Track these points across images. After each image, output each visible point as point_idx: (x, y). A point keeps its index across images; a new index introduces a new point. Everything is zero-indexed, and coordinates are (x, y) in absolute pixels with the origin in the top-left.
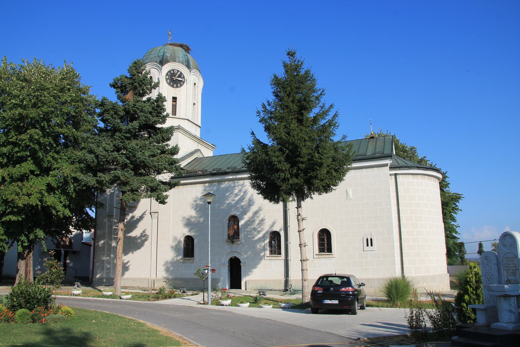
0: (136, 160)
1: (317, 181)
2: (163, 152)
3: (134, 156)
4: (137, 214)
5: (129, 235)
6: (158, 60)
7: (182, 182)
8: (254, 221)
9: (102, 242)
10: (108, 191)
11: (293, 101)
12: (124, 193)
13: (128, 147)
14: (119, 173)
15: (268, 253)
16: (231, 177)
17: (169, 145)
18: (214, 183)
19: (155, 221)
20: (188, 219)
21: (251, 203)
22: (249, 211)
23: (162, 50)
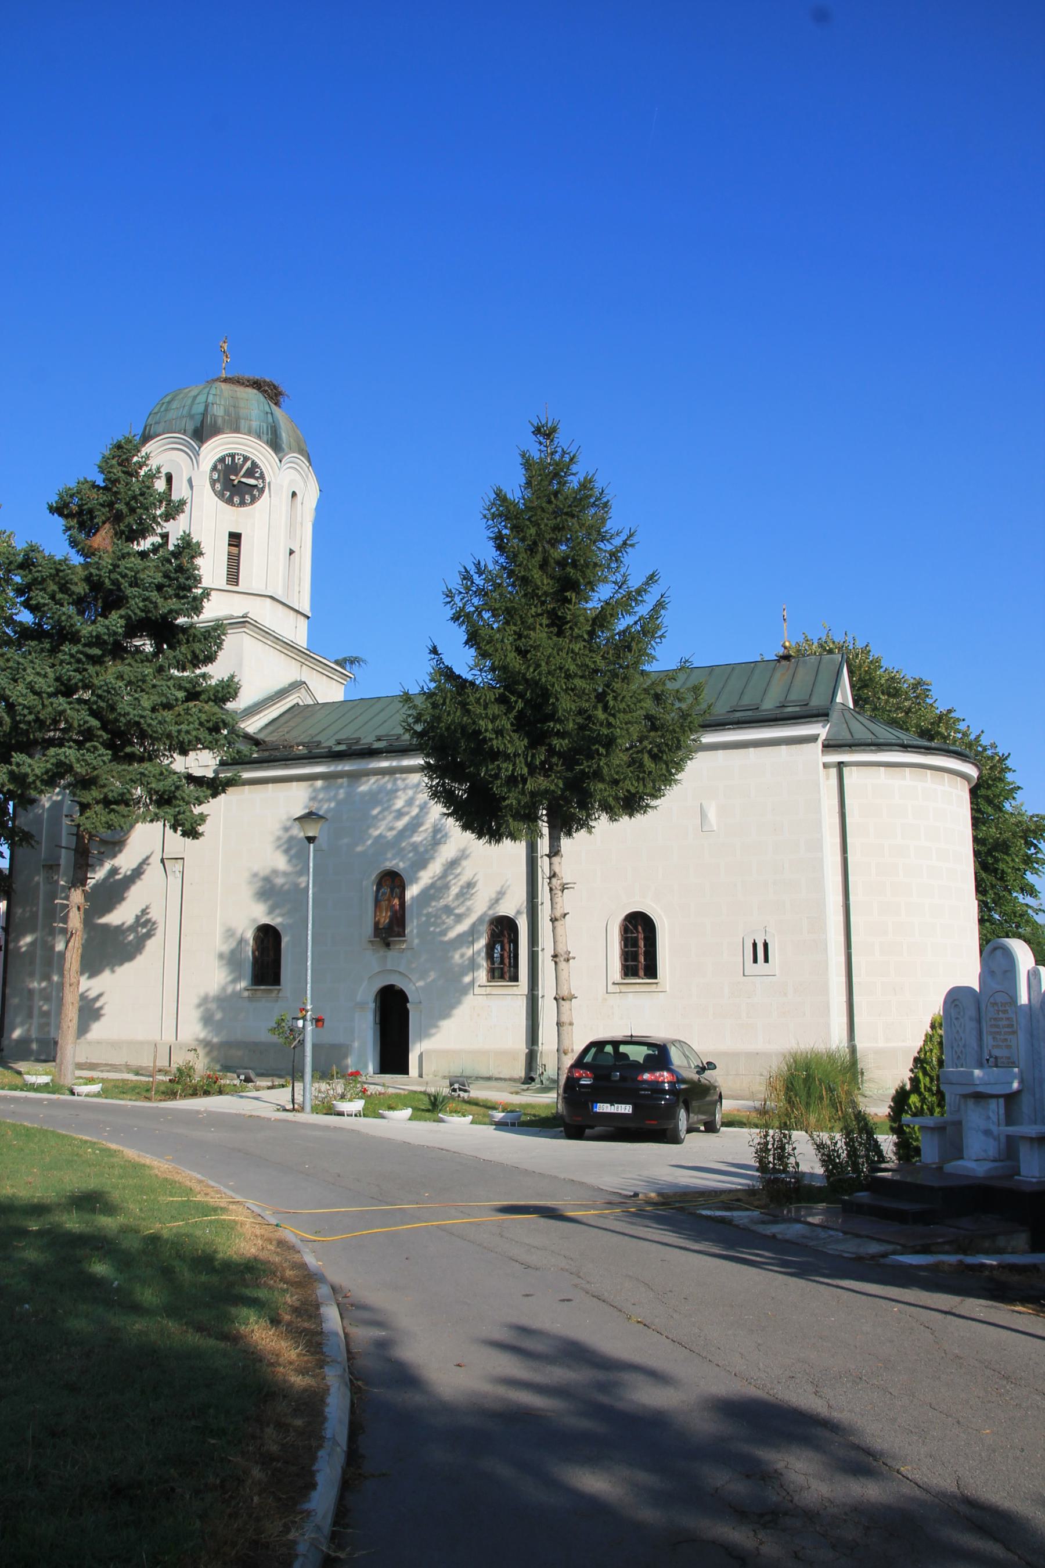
0: (117, 720)
1: (600, 786)
2: (193, 695)
3: (112, 708)
4: (125, 861)
5: (104, 920)
6: (190, 427)
7: (246, 775)
8: (447, 887)
9: (28, 939)
10: (46, 800)
11: (543, 566)
12: (84, 807)
13: (96, 682)
14: (69, 753)
15: (482, 975)
16: (385, 764)
17: (211, 677)
18: (340, 781)
19: (174, 882)
20: (267, 879)
21: (438, 837)
22: (432, 858)
23: (202, 399)
